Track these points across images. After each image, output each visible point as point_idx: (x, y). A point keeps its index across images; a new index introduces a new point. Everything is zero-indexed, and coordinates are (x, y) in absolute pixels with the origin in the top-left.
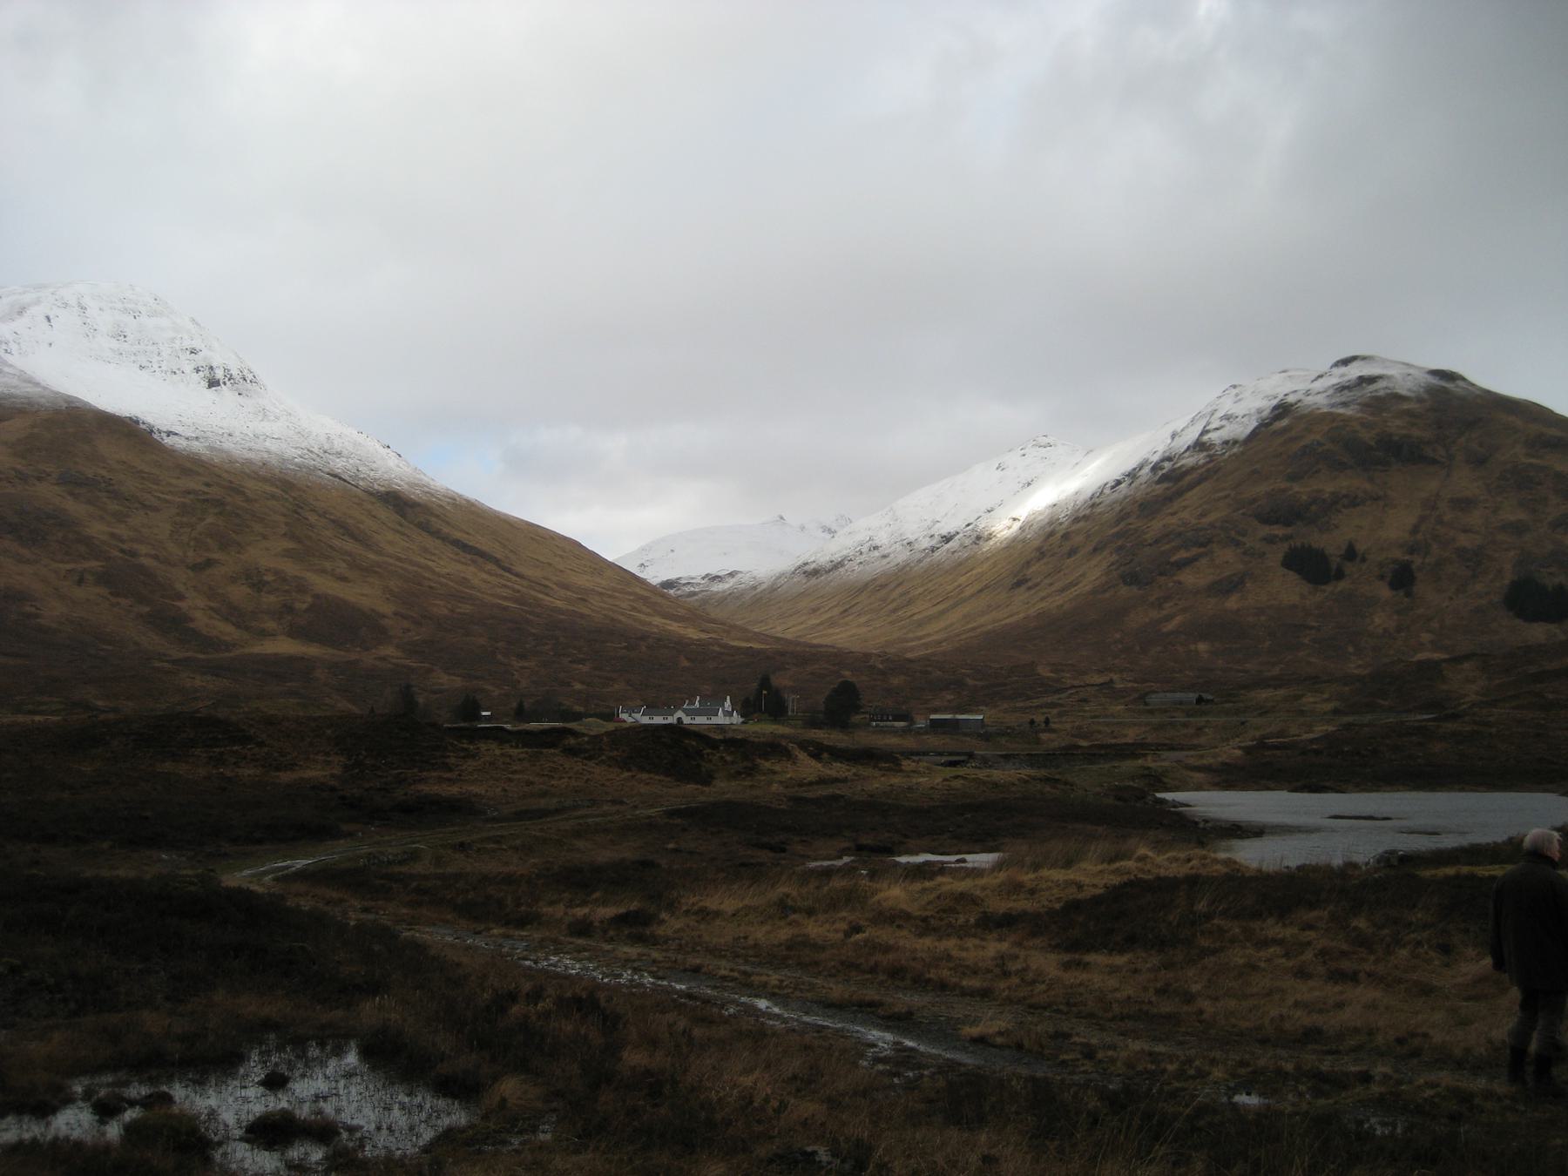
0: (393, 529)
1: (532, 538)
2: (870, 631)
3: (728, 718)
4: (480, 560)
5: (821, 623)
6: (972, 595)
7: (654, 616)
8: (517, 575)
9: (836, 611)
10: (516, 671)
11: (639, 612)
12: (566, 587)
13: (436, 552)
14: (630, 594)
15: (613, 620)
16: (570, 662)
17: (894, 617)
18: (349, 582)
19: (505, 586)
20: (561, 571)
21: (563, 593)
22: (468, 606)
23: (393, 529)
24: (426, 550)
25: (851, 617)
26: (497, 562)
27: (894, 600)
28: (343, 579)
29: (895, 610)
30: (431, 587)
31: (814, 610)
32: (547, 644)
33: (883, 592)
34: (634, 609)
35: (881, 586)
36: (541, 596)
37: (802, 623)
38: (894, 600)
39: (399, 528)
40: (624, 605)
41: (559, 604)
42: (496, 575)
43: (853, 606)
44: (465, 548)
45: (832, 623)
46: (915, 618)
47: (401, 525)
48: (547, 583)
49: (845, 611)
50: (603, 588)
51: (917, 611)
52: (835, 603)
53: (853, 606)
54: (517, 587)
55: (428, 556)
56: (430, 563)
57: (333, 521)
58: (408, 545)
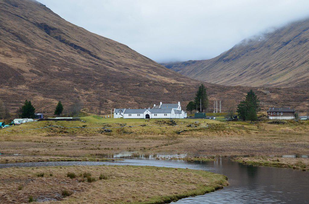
0: (42, 38)
1: (107, 44)
2: (252, 82)
3: (178, 115)
4: (82, 52)
5: (231, 80)
6: (299, 66)
7: (157, 75)
8: (98, 58)
9: (237, 75)
10: (82, 96)
11: (151, 73)
12: (119, 63)
13: (62, 48)
14: (148, 66)
15: (138, 76)
16: (111, 92)
17: (263, 76)
18: (11, 57)
19: (92, 63)
20: (118, 57)
21: (118, 66)
22: (69, 69)
23: (42, 38)
24: (57, 47)
25: (243, 77)
26: (89, 53)
27: (262, 70)
28: (7, 56)
29: (263, 74)
30: (53, 61)
31: (228, 75)
32: (101, 84)
33: (257, 67)
34: (149, 72)
35: (256, 64)
36: (107, 67)
37: (222, 80)
38: (262, 70)
39: (46, 38)
40: (145, 71)
41: (115, 70)
42: (89, 58)
43: (244, 73)
44: (76, 47)
45: (235, 80)
46: (273, 76)
47: (47, 37)
48: (111, 62)
49: (241, 75)
50: (136, 64)
51: (273, 73)
52: (237, 72)
53: (244, 73)
54: (97, 63)
55: (58, 50)
56: (58, 52)
57: (13, 34)
58: (48, 45)
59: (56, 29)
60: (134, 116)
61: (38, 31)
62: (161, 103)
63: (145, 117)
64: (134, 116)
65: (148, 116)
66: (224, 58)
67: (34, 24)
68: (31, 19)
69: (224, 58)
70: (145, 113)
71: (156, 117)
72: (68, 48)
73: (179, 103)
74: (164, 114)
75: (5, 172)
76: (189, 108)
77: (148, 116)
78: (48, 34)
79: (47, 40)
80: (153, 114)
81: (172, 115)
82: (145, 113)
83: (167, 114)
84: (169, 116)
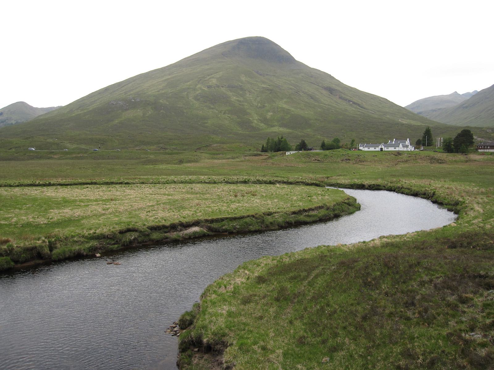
1: (372, 98)
3: (405, 148)
8: (364, 108)
30: (332, 112)
57: (308, 95)
59: (337, 90)
60: (372, 149)
61: (324, 92)
62: (394, 140)
63: (379, 150)
64: (372, 149)
65: (382, 149)
66: (464, 106)
67: (322, 88)
68: (320, 85)
69: (464, 106)
70: (380, 147)
71: (387, 150)
72: (104, 188)
73: (408, 139)
74: (394, 148)
75: (1, 322)
76: (418, 144)
77: (382, 149)
78: (331, 93)
79: (330, 98)
80: (386, 148)
81: (400, 148)
82: (380, 147)
83: (396, 148)
84: (397, 149)
